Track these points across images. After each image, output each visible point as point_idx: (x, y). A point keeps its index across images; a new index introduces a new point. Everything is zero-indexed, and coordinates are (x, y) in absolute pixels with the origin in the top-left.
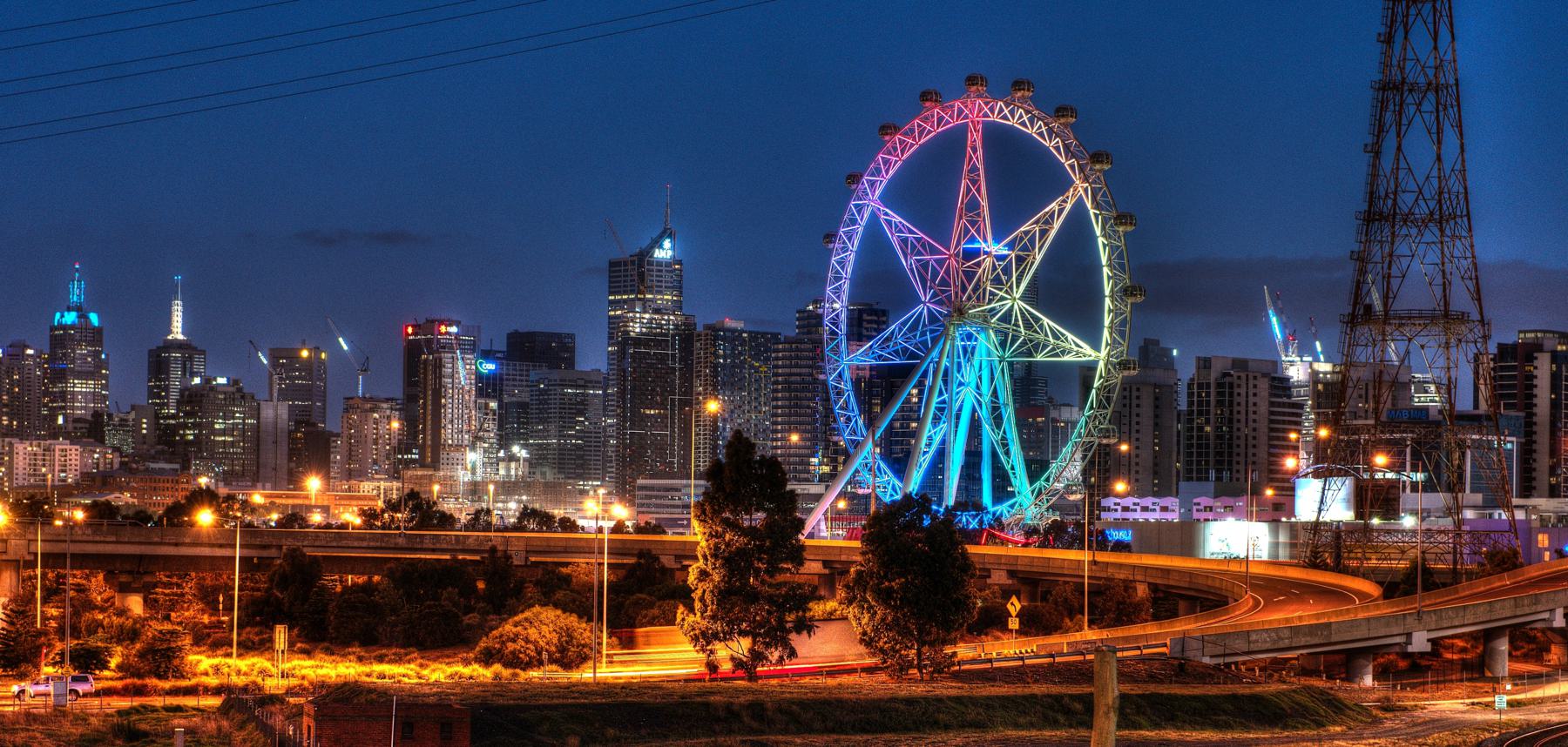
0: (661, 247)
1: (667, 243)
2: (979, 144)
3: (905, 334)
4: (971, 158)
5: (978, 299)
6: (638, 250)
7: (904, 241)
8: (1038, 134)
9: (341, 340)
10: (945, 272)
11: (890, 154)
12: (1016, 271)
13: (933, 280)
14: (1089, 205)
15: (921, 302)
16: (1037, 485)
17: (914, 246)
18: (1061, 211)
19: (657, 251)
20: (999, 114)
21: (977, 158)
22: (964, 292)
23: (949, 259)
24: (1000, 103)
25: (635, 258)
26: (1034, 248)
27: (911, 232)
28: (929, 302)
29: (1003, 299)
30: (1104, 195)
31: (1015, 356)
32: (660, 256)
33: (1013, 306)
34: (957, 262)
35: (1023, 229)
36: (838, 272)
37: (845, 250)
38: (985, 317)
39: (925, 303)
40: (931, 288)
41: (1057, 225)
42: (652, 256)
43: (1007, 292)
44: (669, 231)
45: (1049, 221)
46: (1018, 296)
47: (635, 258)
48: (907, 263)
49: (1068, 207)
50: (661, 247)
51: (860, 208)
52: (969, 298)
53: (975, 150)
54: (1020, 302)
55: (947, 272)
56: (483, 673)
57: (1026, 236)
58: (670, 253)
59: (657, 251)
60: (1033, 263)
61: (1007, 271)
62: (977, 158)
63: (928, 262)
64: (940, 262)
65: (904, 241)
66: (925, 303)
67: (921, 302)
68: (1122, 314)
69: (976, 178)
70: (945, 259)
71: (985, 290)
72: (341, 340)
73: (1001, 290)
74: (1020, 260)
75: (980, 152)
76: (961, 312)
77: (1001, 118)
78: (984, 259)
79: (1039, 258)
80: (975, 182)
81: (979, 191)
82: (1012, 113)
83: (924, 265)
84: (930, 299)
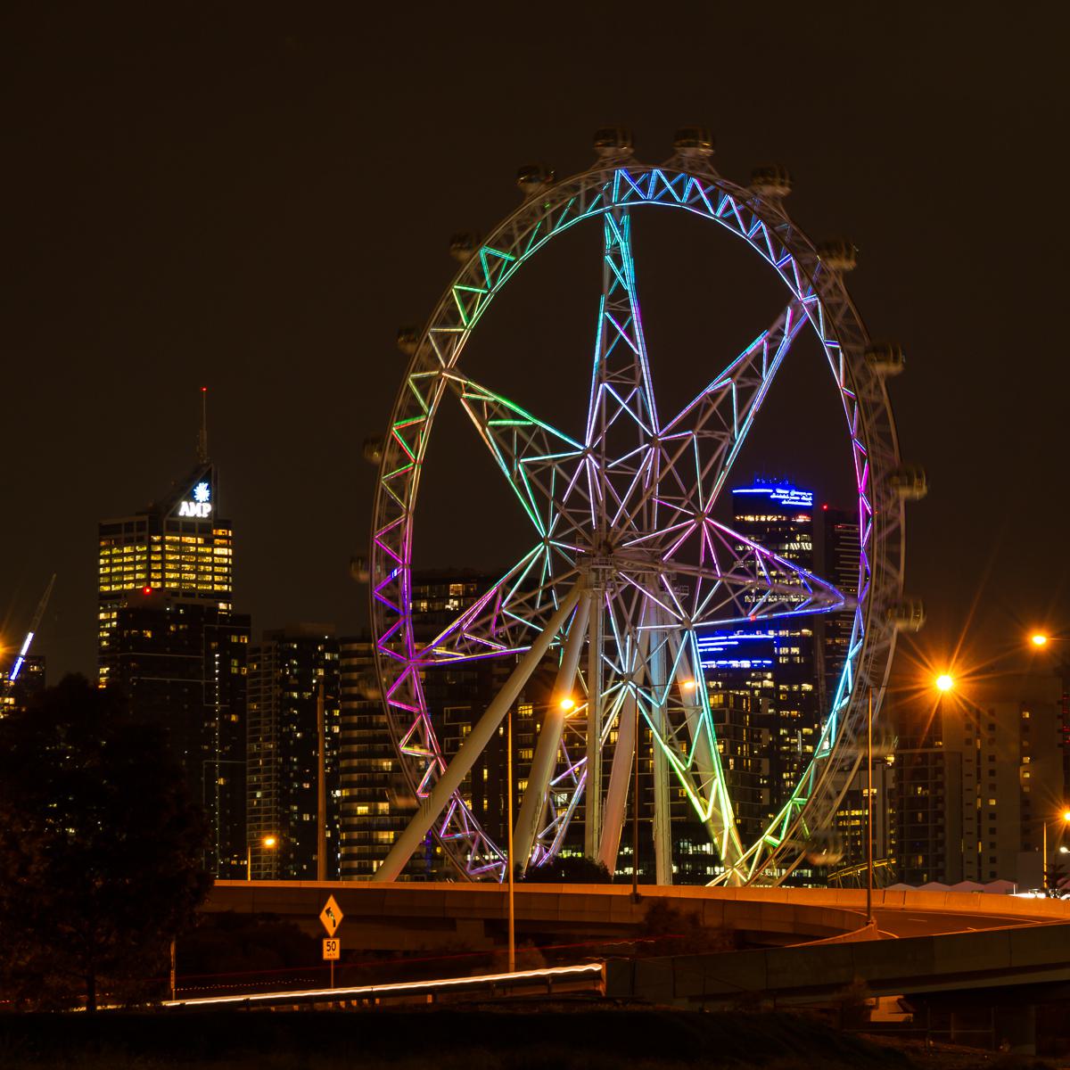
0: (191, 497)
1: (202, 491)
2: (625, 248)
3: (513, 599)
4: (613, 276)
5: (638, 520)
6: (151, 505)
7: (504, 435)
8: (726, 220)
9: (30, 636)
10: (578, 482)
11: (472, 284)
12: (702, 471)
13: (560, 493)
14: (822, 336)
15: (537, 539)
16: (758, 846)
17: (521, 442)
18: (746, 395)
19: (184, 504)
20: (656, 192)
21: (623, 275)
22: (612, 513)
23: (584, 456)
24: (657, 172)
25: (146, 518)
26: (731, 424)
27: (516, 416)
28: (554, 538)
29: (684, 517)
30: (848, 314)
31: (708, 619)
32: (190, 514)
33: (699, 530)
34: (598, 461)
35: (710, 389)
36: (393, 503)
37: (404, 460)
38: (653, 552)
39: (545, 540)
40: (556, 511)
41: (767, 377)
42: (175, 514)
43: (688, 507)
44: (205, 470)
45: (752, 372)
46: (707, 509)
47: (146, 518)
48: (516, 471)
49: (786, 341)
50: (191, 497)
51: (424, 385)
52: (622, 521)
53: (618, 259)
54: (543, 534)
55: (582, 481)
56: (173, 972)
57: (714, 400)
58: (208, 508)
59: (184, 504)
60: (730, 448)
61: (686, 466)
62: (623, 275)
63: (549, 469)
64: (570, 466)
65: (504, 435)
66: (545, 540)
67: (537, 539)
68: (889, 523)
69: (624, 309)
70: (578, 459)
71: (650, 502)
72: (30, 636)
73: (679, 503)
74: (708, 447)
75: (628, 265)
76: (608, 548)
77: (661, 199)
78: (647, 450)
79: (740, 436)
80: (622, 316)
81: (630, 332)
82: (679, 188)
83: (540, 474)
84: (557, 531)
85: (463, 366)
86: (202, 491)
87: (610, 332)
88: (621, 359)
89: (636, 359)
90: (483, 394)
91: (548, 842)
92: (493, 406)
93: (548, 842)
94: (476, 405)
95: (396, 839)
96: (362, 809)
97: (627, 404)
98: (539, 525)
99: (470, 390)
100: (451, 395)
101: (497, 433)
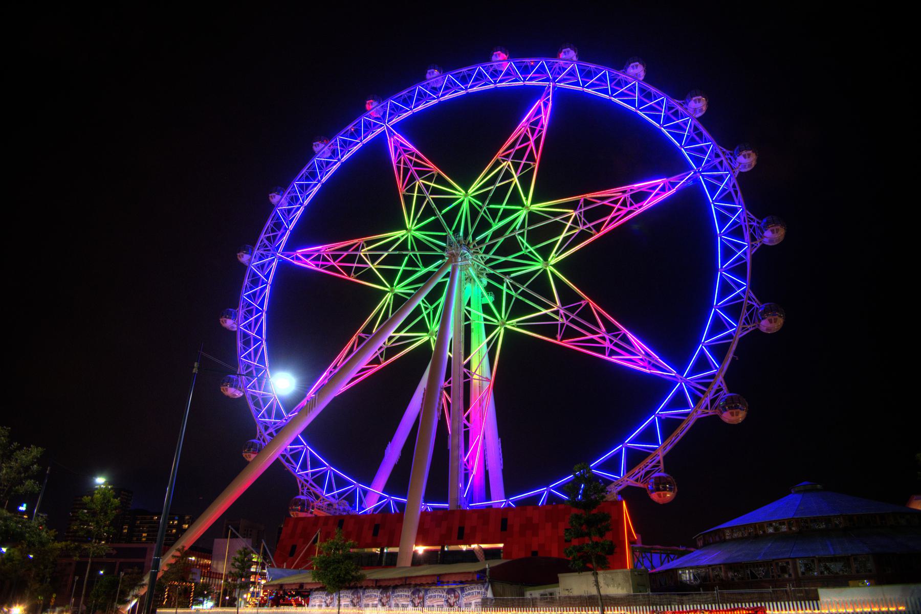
0: (87, 497)
1: (25, 505)
80: (663, 190)
85: (560, 94)
86: (25, 505)
87: (654, 187)
88: (640, 197)
89: (640, 204)
90: (546, 114)
91: (466, 472)
92: (540, 125)
93: (466, 472)
94: (538, 112)
95: (189, 527)
96: (82, 526)
97: (739, 255)
98: (406, 143)
99: (546, 105)
100: (538, 92)
101: (525, 132)
